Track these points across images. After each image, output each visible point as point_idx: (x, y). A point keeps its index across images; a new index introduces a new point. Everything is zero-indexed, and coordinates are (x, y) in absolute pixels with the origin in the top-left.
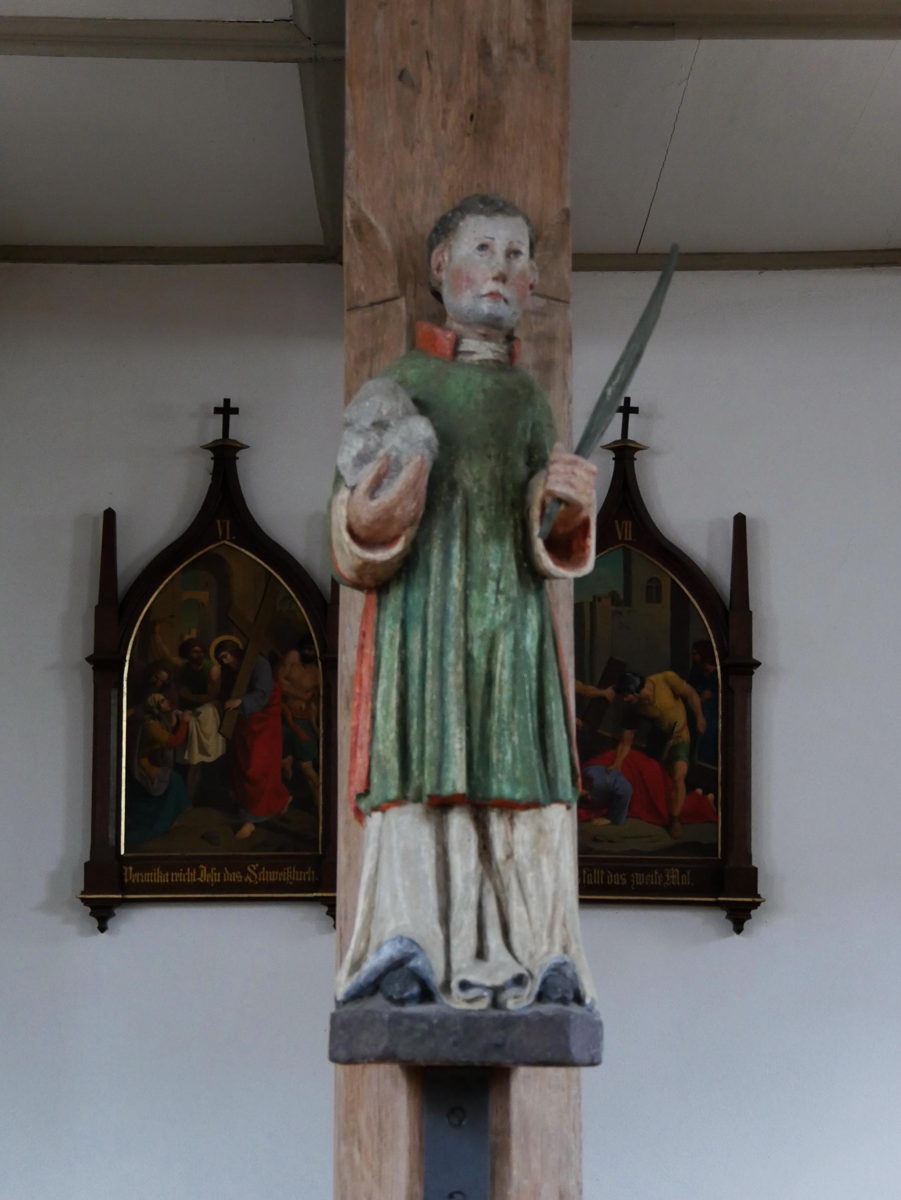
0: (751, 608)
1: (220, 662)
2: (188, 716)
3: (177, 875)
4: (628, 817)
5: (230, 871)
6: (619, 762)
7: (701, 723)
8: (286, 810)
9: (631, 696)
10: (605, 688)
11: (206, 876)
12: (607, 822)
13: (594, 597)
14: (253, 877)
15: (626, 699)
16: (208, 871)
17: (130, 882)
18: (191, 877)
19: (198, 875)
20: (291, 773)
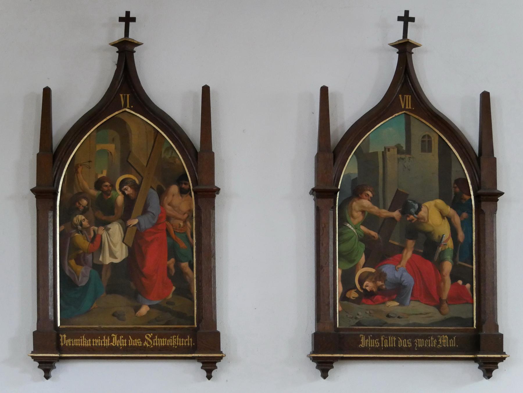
0: (213, 150)
1: (123, 193)
2: (101, 231)
3: (97, 341)
4: (411, 300)
5: (133, 339)
6: (404, 262)
7: (461, 236)
8: (171, 296)
9: (412, 217)
10: (394, 211)
12: (397, 304)
13: (385, 148)
14: (149, 343)
15: (408, 219)
16: (118, 338)
17: (64, 345)
18: (106, 342)
19: (111, 341)
20: (174, 271)
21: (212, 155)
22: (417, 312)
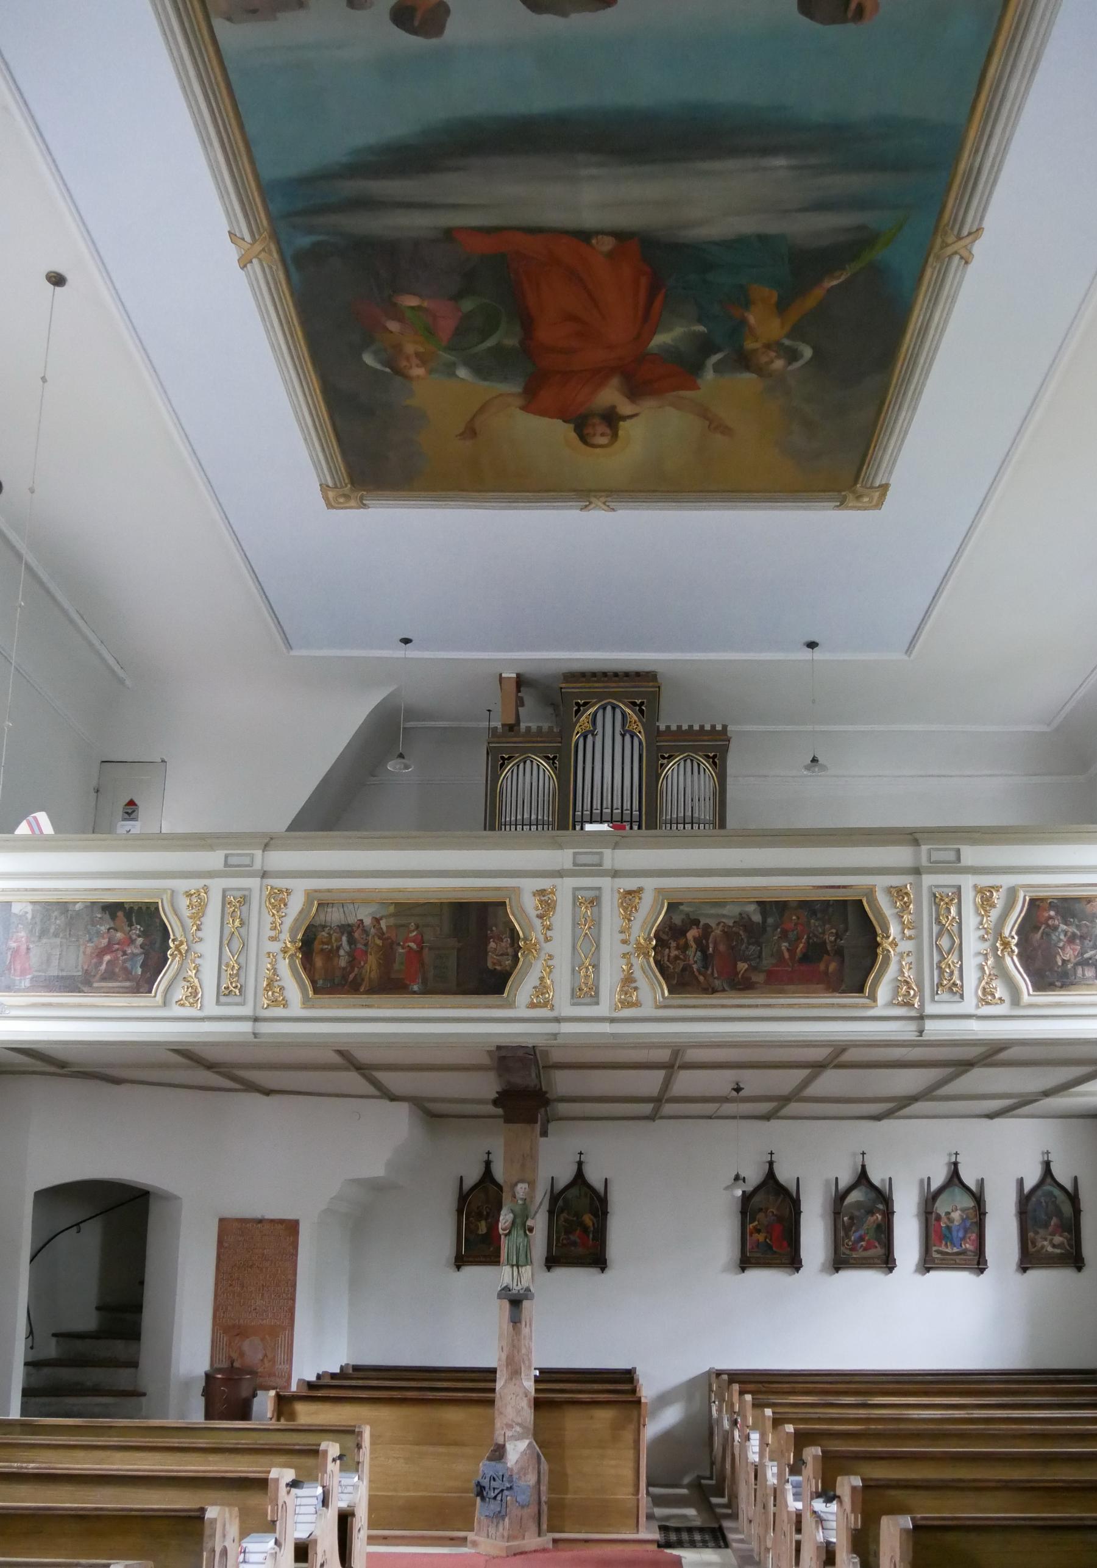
11: (482, 1259)
21: (800, 1201)
22: (580, 1250)
